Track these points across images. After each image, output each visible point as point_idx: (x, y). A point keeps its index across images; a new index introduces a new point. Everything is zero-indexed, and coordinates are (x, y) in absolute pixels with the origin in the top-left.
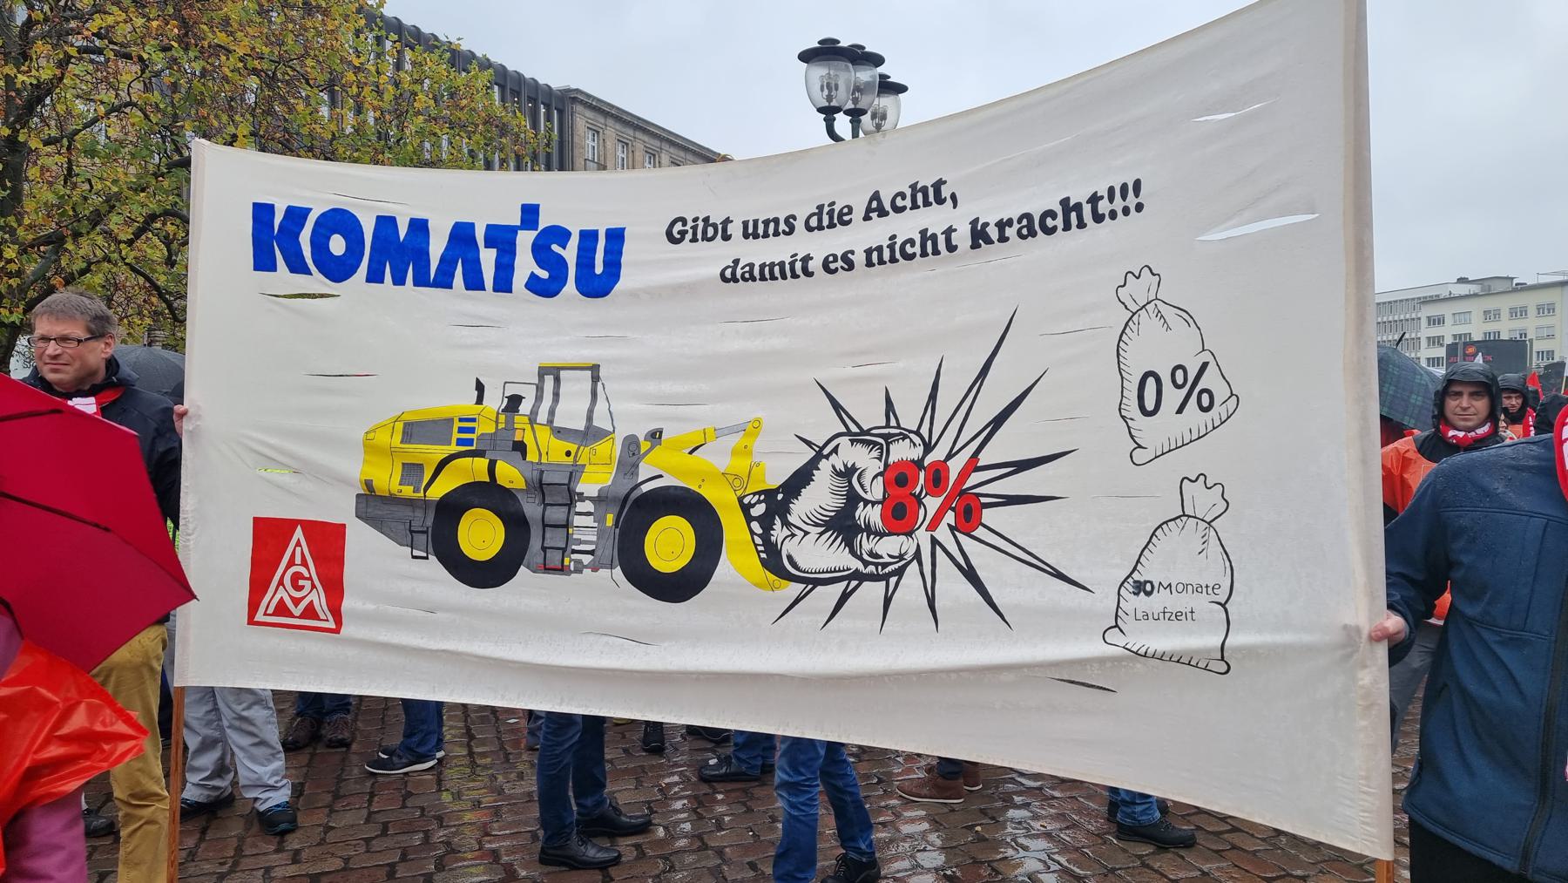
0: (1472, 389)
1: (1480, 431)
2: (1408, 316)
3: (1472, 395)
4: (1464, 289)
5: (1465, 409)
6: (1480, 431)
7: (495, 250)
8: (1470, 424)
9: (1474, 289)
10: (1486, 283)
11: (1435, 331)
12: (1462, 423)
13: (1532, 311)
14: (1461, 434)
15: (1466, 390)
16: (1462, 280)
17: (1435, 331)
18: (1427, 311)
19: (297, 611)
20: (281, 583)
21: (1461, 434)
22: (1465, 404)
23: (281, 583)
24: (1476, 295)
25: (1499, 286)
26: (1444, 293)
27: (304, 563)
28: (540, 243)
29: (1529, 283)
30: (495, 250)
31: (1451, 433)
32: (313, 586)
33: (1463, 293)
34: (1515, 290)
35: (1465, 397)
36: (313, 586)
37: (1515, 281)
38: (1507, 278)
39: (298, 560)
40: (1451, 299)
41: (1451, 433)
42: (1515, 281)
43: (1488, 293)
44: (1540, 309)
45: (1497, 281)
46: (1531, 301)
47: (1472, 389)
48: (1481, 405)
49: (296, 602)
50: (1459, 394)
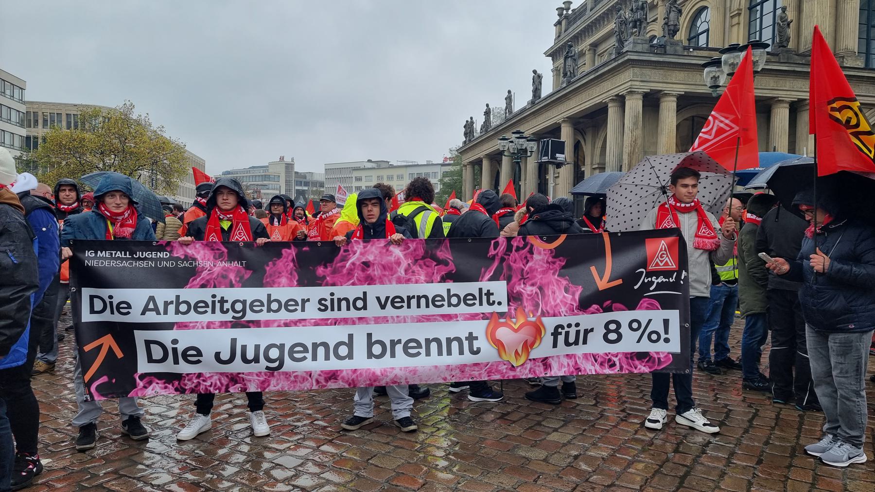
0: (69, 188)
1: (74, 205)
2: (348, 176)
3: (70, 190)
4: (370, 165)
5: (68, 196)
6: (74, 205)
7: (83, 321)
8: (70, 202)
9: (374, 165)
10: (379, 163)
11: (358, 184)
12: (67, 202)
13: (395, 178)
14: (66, 207)
15: (67, 188)
16: (369, 161)
17: (358, 184)
18: (356, 174)
19: (661, 264)
20: (658, 257)
21: (66, 207)
22: (67, 194)
23: (658, 257)
24: (374, 168)
25: (383, 165)
26: (362, 167)
27: (665, 250)
28: (605, 115)
29: (395, 164)
30: (83, 321)
31: (62, 207)
32: (667, 256)
33: (369, 167)
34: (389, 168)
35: (67, 191)
36: (667, 256)
37: (390, 163)
38: (387, 162)
39: (663, 249)
40: (364, 169)
41: (62, 207)
42: (390, 163)
43: (379, 168)
44: (398, 177)
45: (383, 163)
46: (395, 173)
47: (69, 188)
48: (73, 194)
49: (661, 261)
50: (65, 190)
